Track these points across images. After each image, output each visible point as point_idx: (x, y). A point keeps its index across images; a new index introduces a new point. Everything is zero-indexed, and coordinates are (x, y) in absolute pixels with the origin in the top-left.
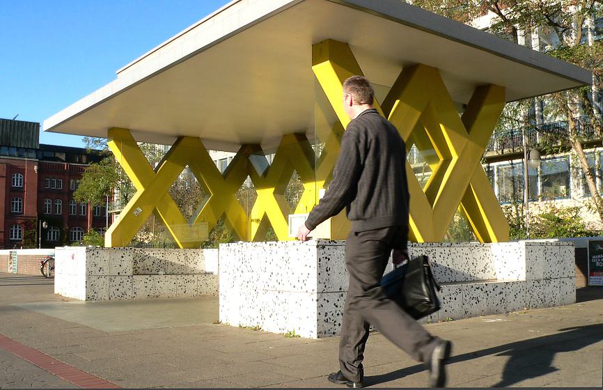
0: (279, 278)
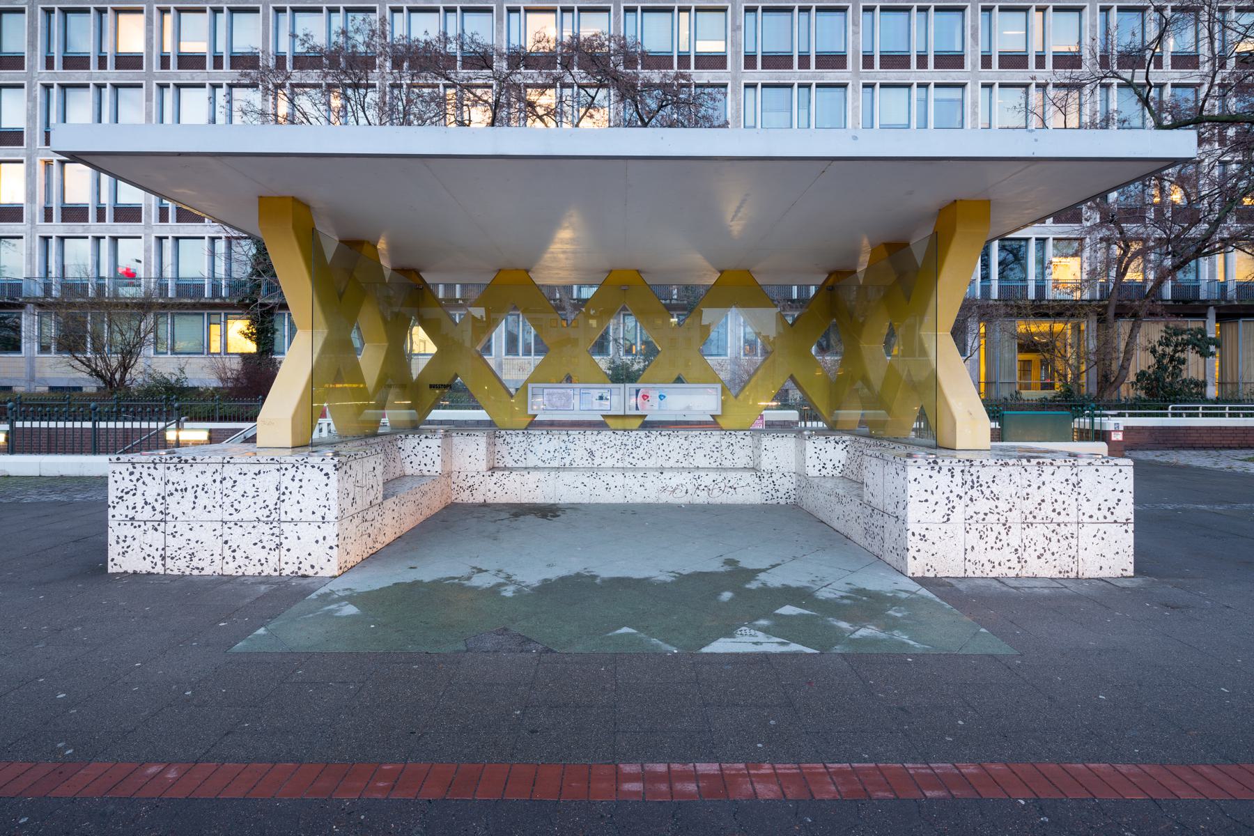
0: (1058, 507)
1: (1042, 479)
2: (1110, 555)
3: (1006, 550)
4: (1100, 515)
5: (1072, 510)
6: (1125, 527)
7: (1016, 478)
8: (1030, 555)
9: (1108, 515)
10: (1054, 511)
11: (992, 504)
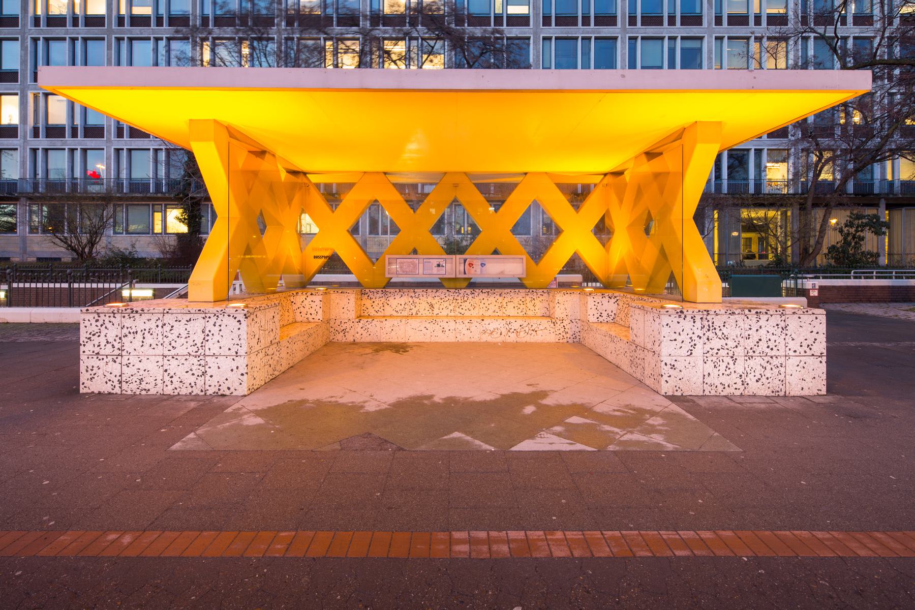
0: (771, 344)
1: (760, 324)
2: (809, 379)
3: (734, 376)
4: (802, 350)
5: (782, 346)
6: (820, 359)
7: (740, 323)
8: (751, 380)
9: (808, 350)
10: (768, 347)
11: (723, 342)
